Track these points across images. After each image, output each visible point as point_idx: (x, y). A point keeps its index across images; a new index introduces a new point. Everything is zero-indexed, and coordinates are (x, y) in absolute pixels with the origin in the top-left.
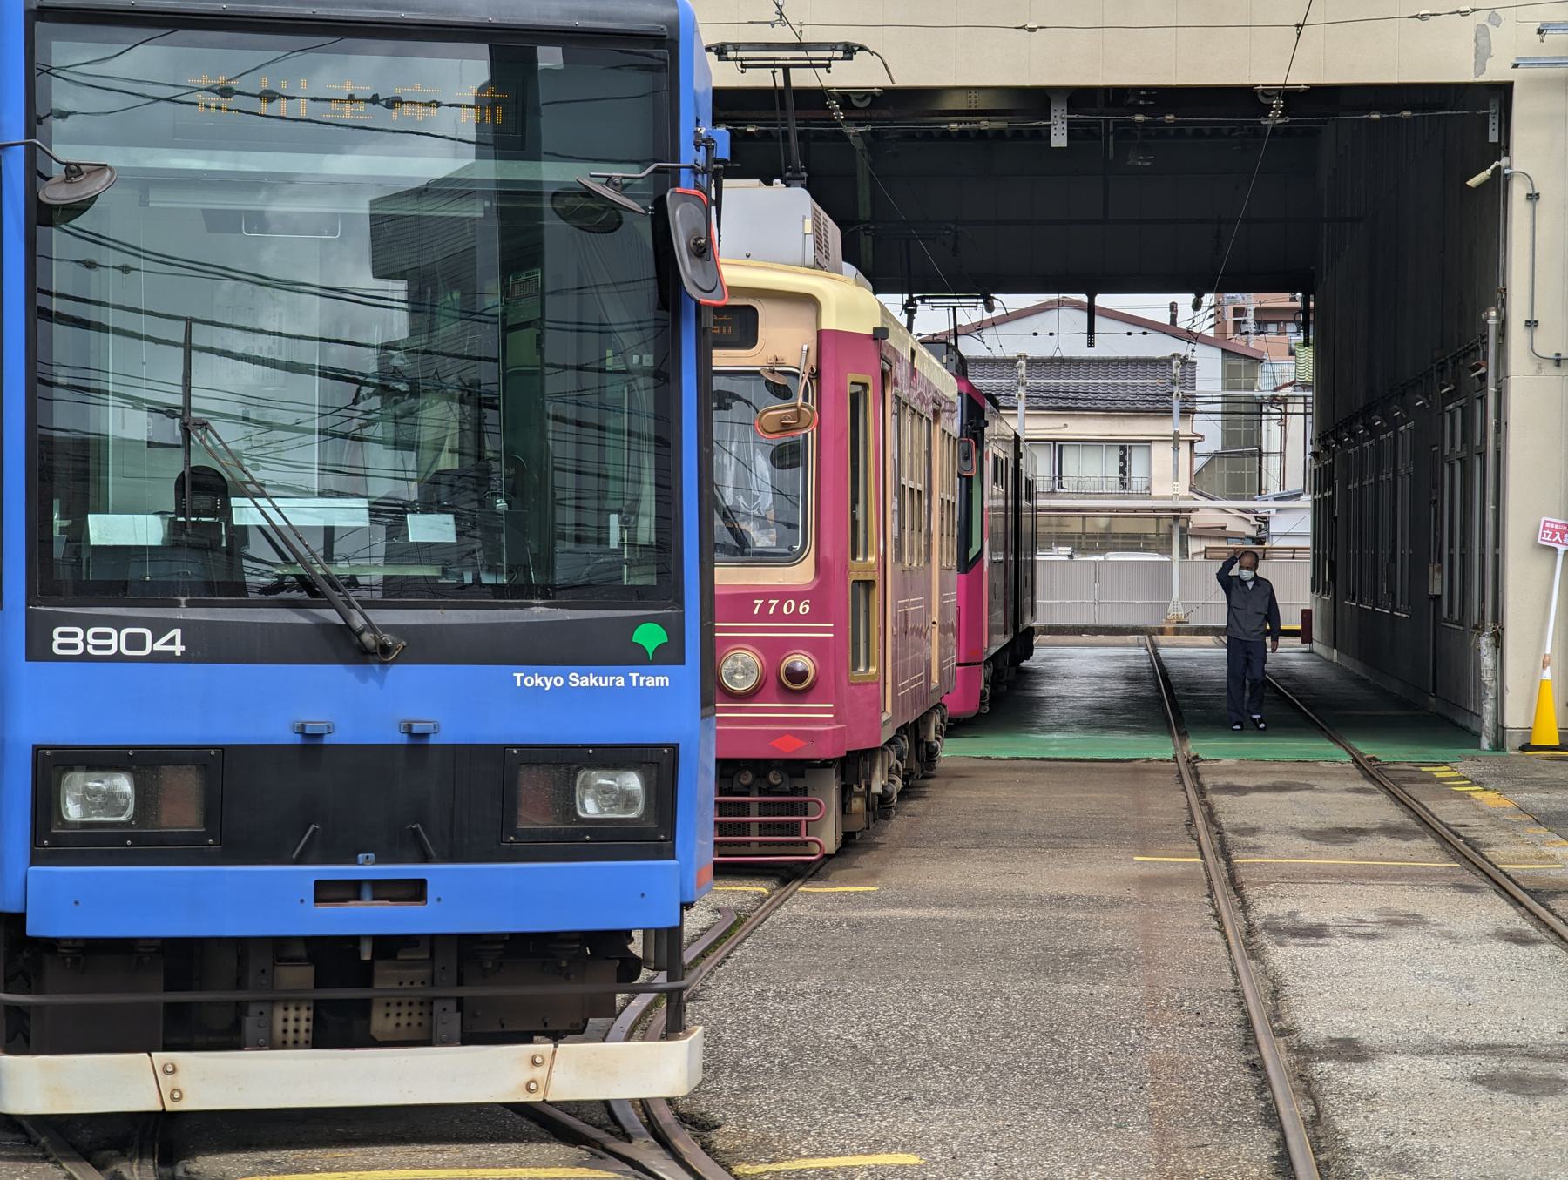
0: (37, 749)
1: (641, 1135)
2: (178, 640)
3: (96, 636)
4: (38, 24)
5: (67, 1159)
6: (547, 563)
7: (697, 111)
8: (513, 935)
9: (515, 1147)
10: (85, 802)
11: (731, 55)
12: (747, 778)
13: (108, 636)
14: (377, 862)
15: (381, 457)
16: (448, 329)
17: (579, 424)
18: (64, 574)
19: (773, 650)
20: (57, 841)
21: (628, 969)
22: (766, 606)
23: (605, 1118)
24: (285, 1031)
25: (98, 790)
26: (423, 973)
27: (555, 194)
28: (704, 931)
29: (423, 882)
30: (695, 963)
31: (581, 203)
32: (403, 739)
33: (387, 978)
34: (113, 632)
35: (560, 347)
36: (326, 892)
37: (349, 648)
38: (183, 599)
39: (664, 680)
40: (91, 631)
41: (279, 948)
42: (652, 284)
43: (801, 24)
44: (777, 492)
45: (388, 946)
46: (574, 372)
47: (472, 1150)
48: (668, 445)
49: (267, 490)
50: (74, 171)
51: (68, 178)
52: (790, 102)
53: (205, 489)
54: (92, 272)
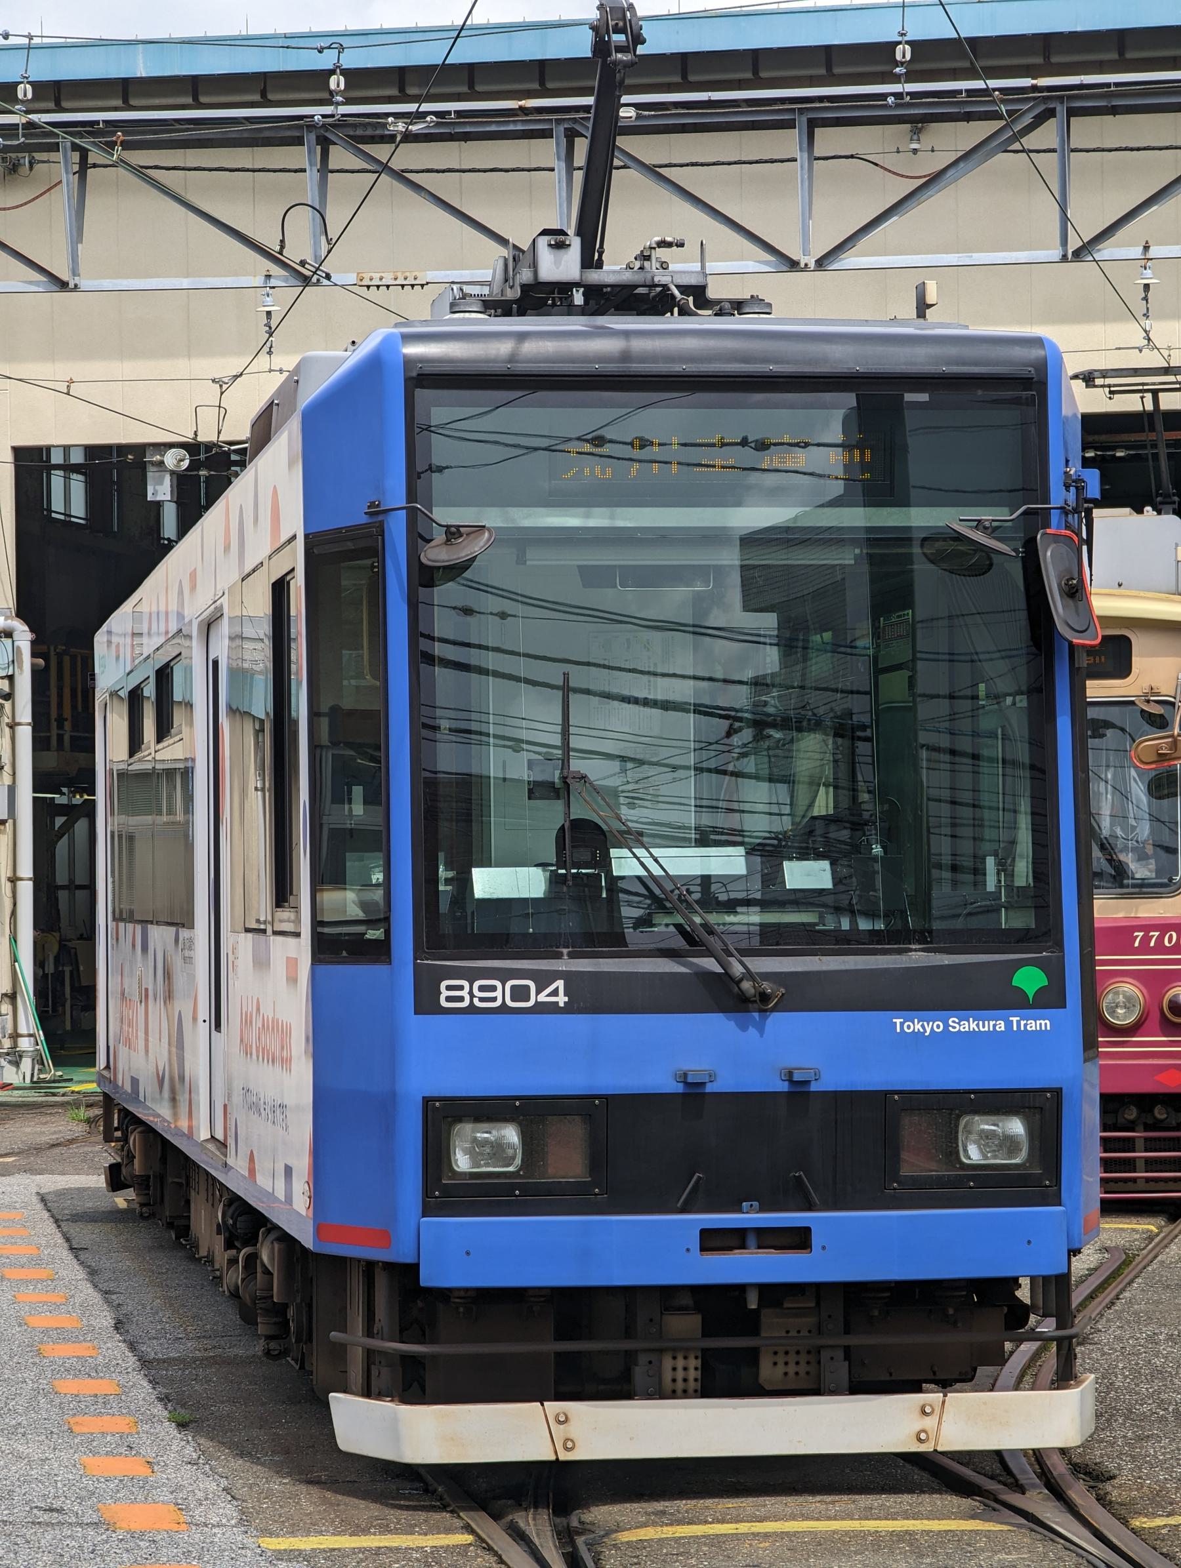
0: (427, 1101)
1: (1034, 1486)
2: (561, 991)
3: (482, 988)
4: (418, 392)
5: (464, 1509)
6: (923, 903)
7: (1066, 450)
8: (899, 1283)
9: (906, 1497)
10: (476, 1149)
11: (1098, 382)
12: (1132, 1114)
13: (494, 988)
14: (762, 1210)
15: (757, 794)
16: (820, 666)
17: (953, 752)
18: (447, 928)
19: (1155, 982)
20: (447, 1191)
21: (1017, 1316)
22: (1146, 939)
23: (997, 1468)
24: (674, 1380)
25: (486, 1141)
26: (811, 1320)
27: (924, 539)
28: (1092, 1271)
29: (807, 1231)
30: (1083, 1305)
31: (952, 546)
32: (784, 1087)
33: (773, 1326)
34: (498, 984)
35: (931, 677)
36: (712, 1240)
37: (729, 997)
38: (565, 951)
39: (1045, 1024)
40: (477, 984)
41: (667, 1297)
42: (1023, 616)
43: (1169, 348)
44: (1155, 819)
45: (773, 1294)
46: (947, 701)
47: (864, 1500)
48: (1043, 772)
49: (645, 839)
50: (453, 533)
51: (448, 540)
52: (1159, 425)
53: (585, 841)
54: (469, 618)
